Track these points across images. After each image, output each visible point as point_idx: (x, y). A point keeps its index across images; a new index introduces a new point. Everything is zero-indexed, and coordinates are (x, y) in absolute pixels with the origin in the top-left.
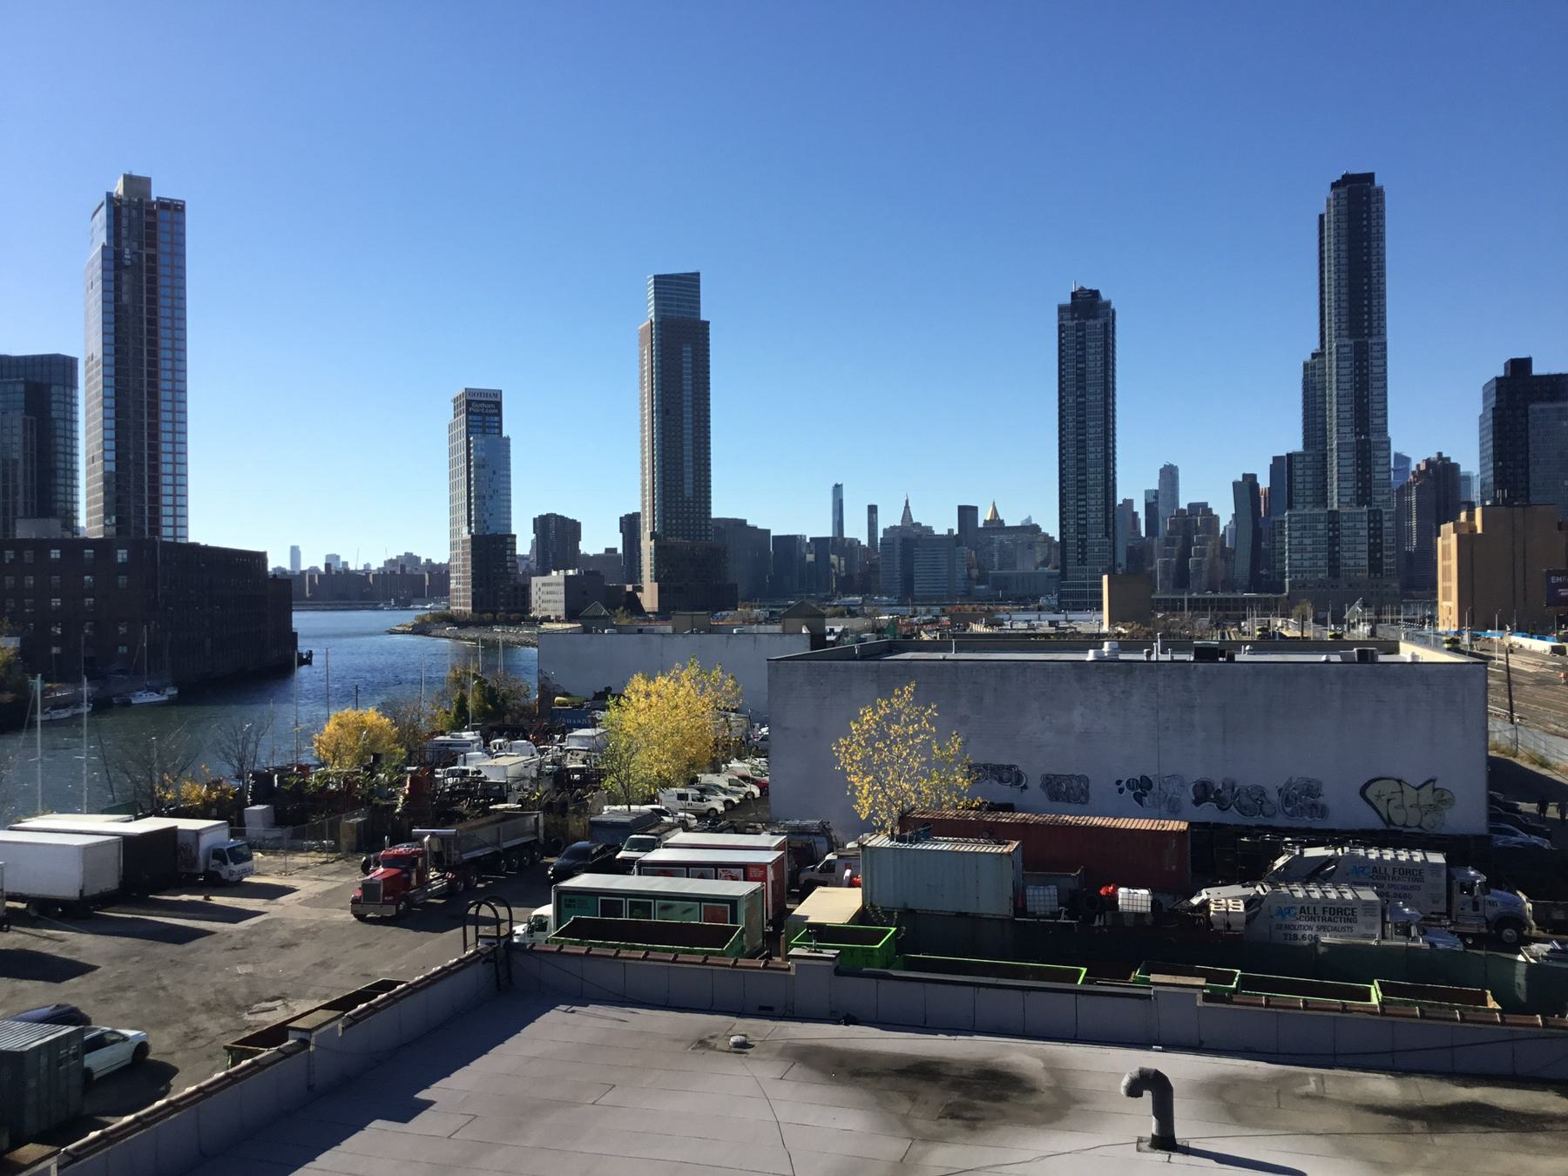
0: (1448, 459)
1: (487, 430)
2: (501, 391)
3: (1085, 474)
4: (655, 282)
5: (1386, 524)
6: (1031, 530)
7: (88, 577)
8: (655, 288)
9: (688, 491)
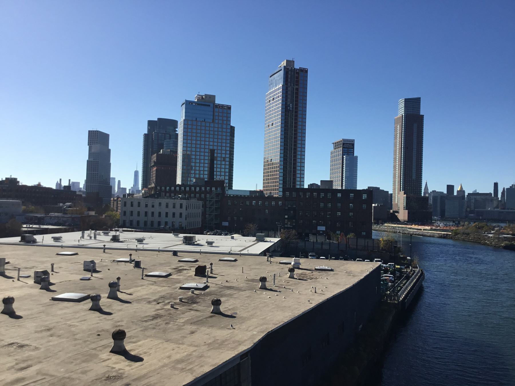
1: (349, 154)
2: (354, 140)
4: (405, 101)
7: (351, 205)
8: (405, 103)
9: (414, 177)
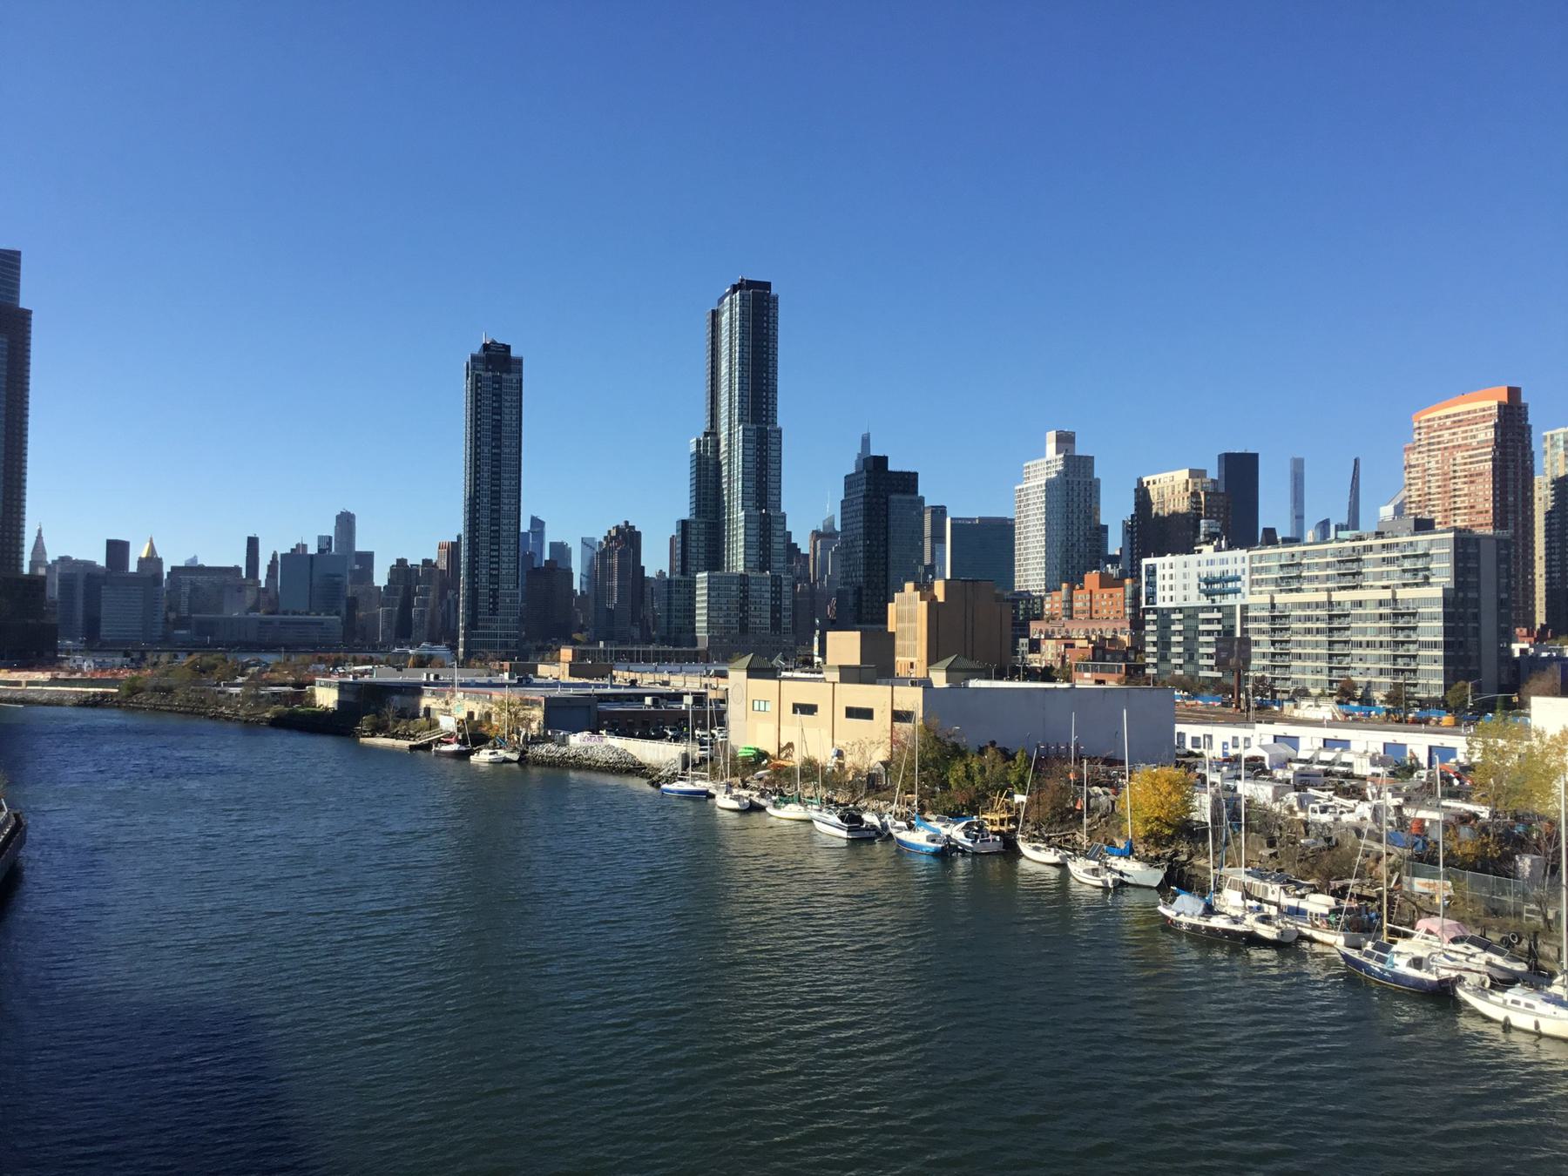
0: (633, 527)
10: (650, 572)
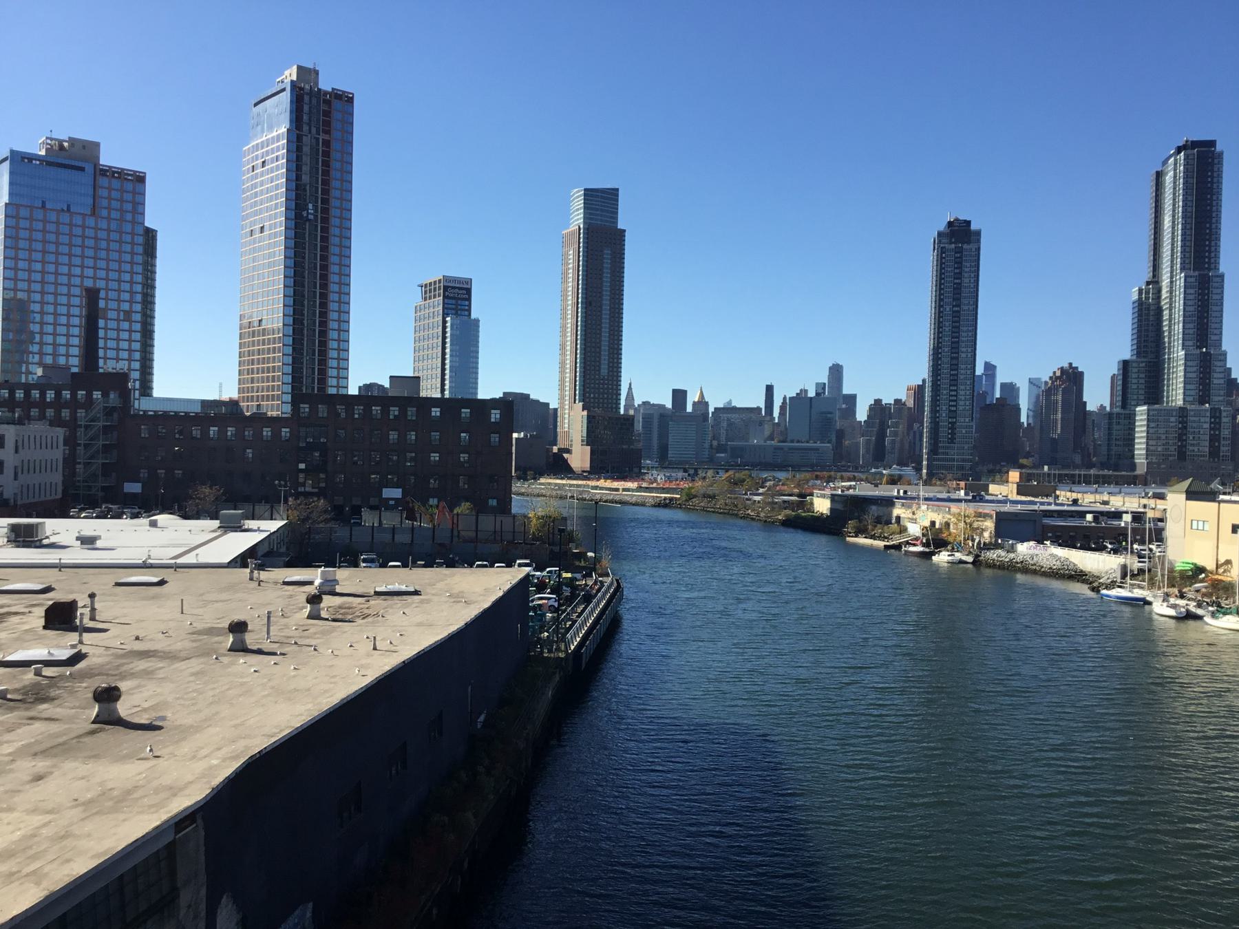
0: (1077, 368)
3: (957, 370)
4: (585, 195)
5: (1224, 420)
6: (663, 407)
7: (464, 435)
9: (604, 371)
10: (1091, 406)
